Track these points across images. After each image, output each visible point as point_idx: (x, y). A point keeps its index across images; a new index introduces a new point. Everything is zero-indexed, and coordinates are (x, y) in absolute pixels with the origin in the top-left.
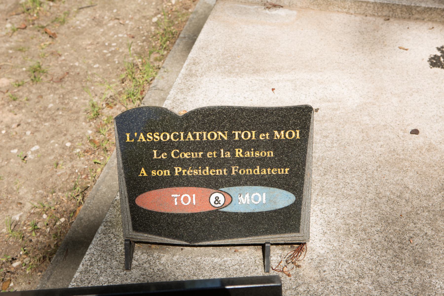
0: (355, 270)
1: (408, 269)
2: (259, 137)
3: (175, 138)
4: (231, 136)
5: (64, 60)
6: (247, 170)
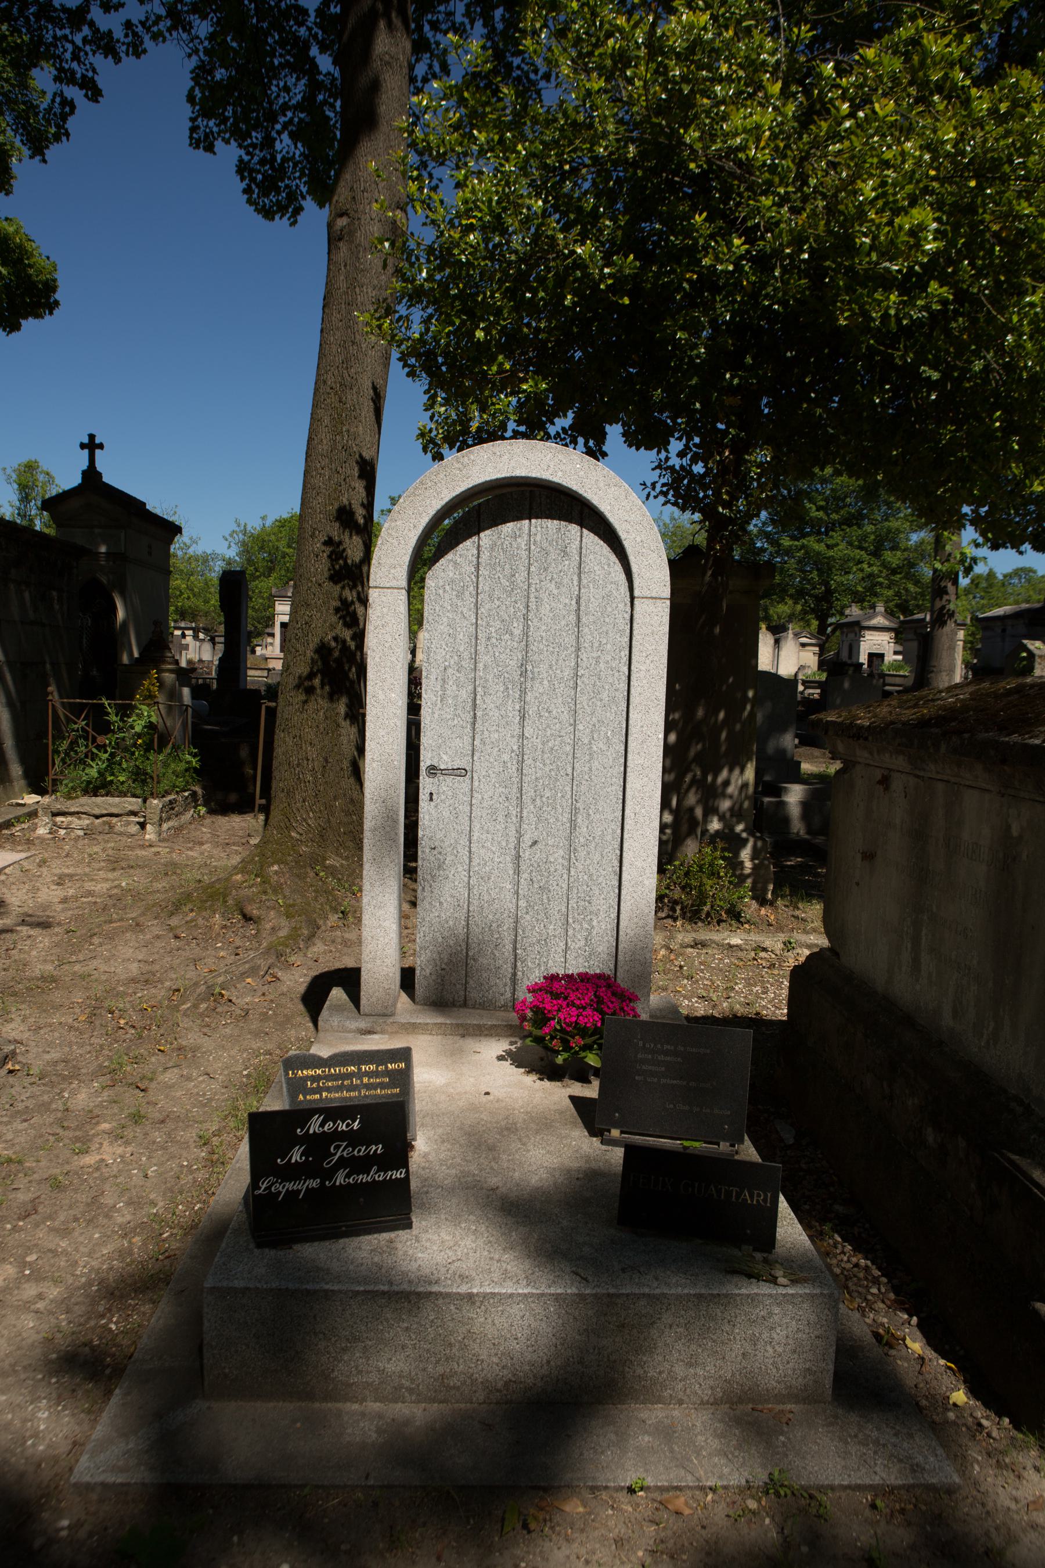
4: (360, 1069)
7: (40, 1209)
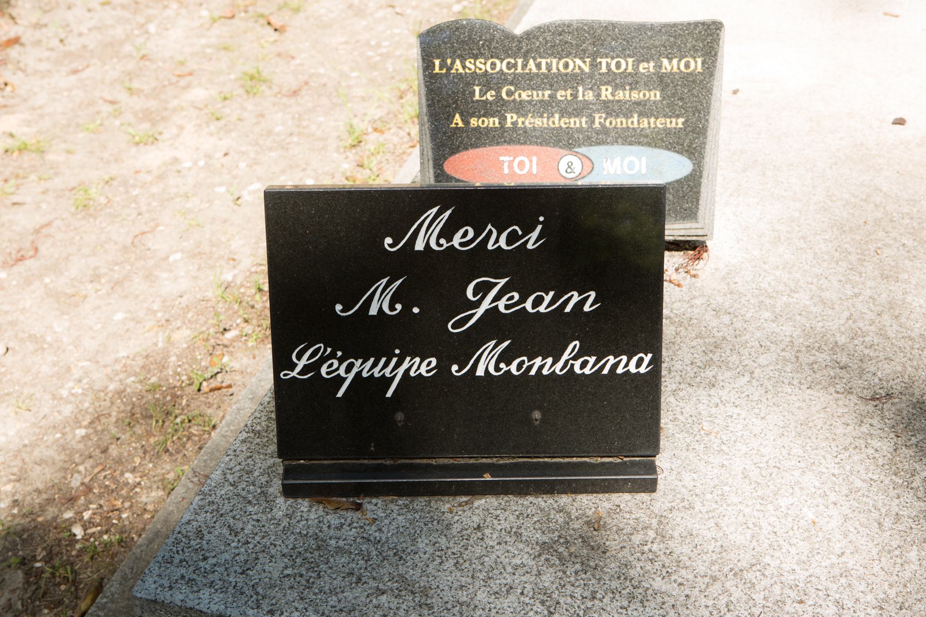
0: (785, 283)
1: (870, 284)
2: (638, 67)
3: (509, 68)
4: (595, 66)
5: (300, 64)
6: (619, 120)
7: (43, 250)
